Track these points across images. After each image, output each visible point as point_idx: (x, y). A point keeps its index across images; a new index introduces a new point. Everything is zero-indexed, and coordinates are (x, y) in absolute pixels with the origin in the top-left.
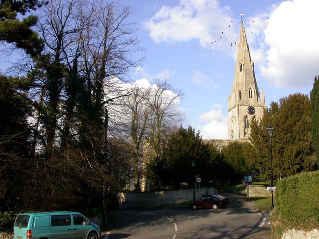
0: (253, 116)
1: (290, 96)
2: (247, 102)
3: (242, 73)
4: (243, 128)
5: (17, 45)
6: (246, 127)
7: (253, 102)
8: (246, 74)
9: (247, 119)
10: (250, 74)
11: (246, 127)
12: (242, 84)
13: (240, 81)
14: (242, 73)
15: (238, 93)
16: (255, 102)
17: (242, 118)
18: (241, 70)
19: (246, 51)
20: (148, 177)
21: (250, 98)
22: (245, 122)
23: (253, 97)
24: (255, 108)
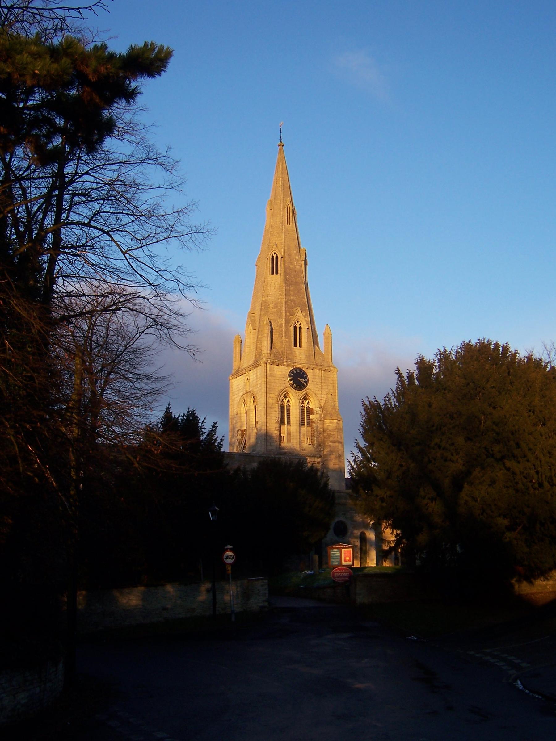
0: (301, 393)
1: (467, 347)
2: (290, 358)
3: (278, 279)
4: (277, 425)
5: (313, 410)
6: (282, 422)
7: (303, 357)
8: (287, 282)
9: (286, 401)
10: (297, 284)
11: (282, 422)
12: (276, 307)
13: (271, 299)
14: (278, 279)
15: (267, 331)
16: (308, 357)
17: (273, 396)
18: (275, 270)
19: (288, 222)
20: (52, 477)
21: (295, 345)
22: (282, 407)
23: (279, 272)
24: (309, 373)
